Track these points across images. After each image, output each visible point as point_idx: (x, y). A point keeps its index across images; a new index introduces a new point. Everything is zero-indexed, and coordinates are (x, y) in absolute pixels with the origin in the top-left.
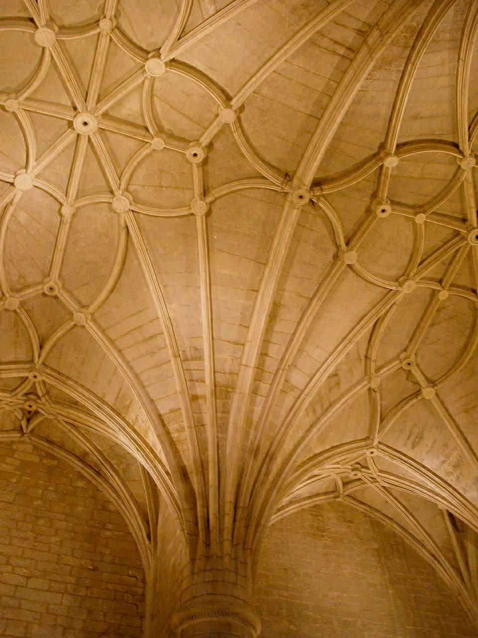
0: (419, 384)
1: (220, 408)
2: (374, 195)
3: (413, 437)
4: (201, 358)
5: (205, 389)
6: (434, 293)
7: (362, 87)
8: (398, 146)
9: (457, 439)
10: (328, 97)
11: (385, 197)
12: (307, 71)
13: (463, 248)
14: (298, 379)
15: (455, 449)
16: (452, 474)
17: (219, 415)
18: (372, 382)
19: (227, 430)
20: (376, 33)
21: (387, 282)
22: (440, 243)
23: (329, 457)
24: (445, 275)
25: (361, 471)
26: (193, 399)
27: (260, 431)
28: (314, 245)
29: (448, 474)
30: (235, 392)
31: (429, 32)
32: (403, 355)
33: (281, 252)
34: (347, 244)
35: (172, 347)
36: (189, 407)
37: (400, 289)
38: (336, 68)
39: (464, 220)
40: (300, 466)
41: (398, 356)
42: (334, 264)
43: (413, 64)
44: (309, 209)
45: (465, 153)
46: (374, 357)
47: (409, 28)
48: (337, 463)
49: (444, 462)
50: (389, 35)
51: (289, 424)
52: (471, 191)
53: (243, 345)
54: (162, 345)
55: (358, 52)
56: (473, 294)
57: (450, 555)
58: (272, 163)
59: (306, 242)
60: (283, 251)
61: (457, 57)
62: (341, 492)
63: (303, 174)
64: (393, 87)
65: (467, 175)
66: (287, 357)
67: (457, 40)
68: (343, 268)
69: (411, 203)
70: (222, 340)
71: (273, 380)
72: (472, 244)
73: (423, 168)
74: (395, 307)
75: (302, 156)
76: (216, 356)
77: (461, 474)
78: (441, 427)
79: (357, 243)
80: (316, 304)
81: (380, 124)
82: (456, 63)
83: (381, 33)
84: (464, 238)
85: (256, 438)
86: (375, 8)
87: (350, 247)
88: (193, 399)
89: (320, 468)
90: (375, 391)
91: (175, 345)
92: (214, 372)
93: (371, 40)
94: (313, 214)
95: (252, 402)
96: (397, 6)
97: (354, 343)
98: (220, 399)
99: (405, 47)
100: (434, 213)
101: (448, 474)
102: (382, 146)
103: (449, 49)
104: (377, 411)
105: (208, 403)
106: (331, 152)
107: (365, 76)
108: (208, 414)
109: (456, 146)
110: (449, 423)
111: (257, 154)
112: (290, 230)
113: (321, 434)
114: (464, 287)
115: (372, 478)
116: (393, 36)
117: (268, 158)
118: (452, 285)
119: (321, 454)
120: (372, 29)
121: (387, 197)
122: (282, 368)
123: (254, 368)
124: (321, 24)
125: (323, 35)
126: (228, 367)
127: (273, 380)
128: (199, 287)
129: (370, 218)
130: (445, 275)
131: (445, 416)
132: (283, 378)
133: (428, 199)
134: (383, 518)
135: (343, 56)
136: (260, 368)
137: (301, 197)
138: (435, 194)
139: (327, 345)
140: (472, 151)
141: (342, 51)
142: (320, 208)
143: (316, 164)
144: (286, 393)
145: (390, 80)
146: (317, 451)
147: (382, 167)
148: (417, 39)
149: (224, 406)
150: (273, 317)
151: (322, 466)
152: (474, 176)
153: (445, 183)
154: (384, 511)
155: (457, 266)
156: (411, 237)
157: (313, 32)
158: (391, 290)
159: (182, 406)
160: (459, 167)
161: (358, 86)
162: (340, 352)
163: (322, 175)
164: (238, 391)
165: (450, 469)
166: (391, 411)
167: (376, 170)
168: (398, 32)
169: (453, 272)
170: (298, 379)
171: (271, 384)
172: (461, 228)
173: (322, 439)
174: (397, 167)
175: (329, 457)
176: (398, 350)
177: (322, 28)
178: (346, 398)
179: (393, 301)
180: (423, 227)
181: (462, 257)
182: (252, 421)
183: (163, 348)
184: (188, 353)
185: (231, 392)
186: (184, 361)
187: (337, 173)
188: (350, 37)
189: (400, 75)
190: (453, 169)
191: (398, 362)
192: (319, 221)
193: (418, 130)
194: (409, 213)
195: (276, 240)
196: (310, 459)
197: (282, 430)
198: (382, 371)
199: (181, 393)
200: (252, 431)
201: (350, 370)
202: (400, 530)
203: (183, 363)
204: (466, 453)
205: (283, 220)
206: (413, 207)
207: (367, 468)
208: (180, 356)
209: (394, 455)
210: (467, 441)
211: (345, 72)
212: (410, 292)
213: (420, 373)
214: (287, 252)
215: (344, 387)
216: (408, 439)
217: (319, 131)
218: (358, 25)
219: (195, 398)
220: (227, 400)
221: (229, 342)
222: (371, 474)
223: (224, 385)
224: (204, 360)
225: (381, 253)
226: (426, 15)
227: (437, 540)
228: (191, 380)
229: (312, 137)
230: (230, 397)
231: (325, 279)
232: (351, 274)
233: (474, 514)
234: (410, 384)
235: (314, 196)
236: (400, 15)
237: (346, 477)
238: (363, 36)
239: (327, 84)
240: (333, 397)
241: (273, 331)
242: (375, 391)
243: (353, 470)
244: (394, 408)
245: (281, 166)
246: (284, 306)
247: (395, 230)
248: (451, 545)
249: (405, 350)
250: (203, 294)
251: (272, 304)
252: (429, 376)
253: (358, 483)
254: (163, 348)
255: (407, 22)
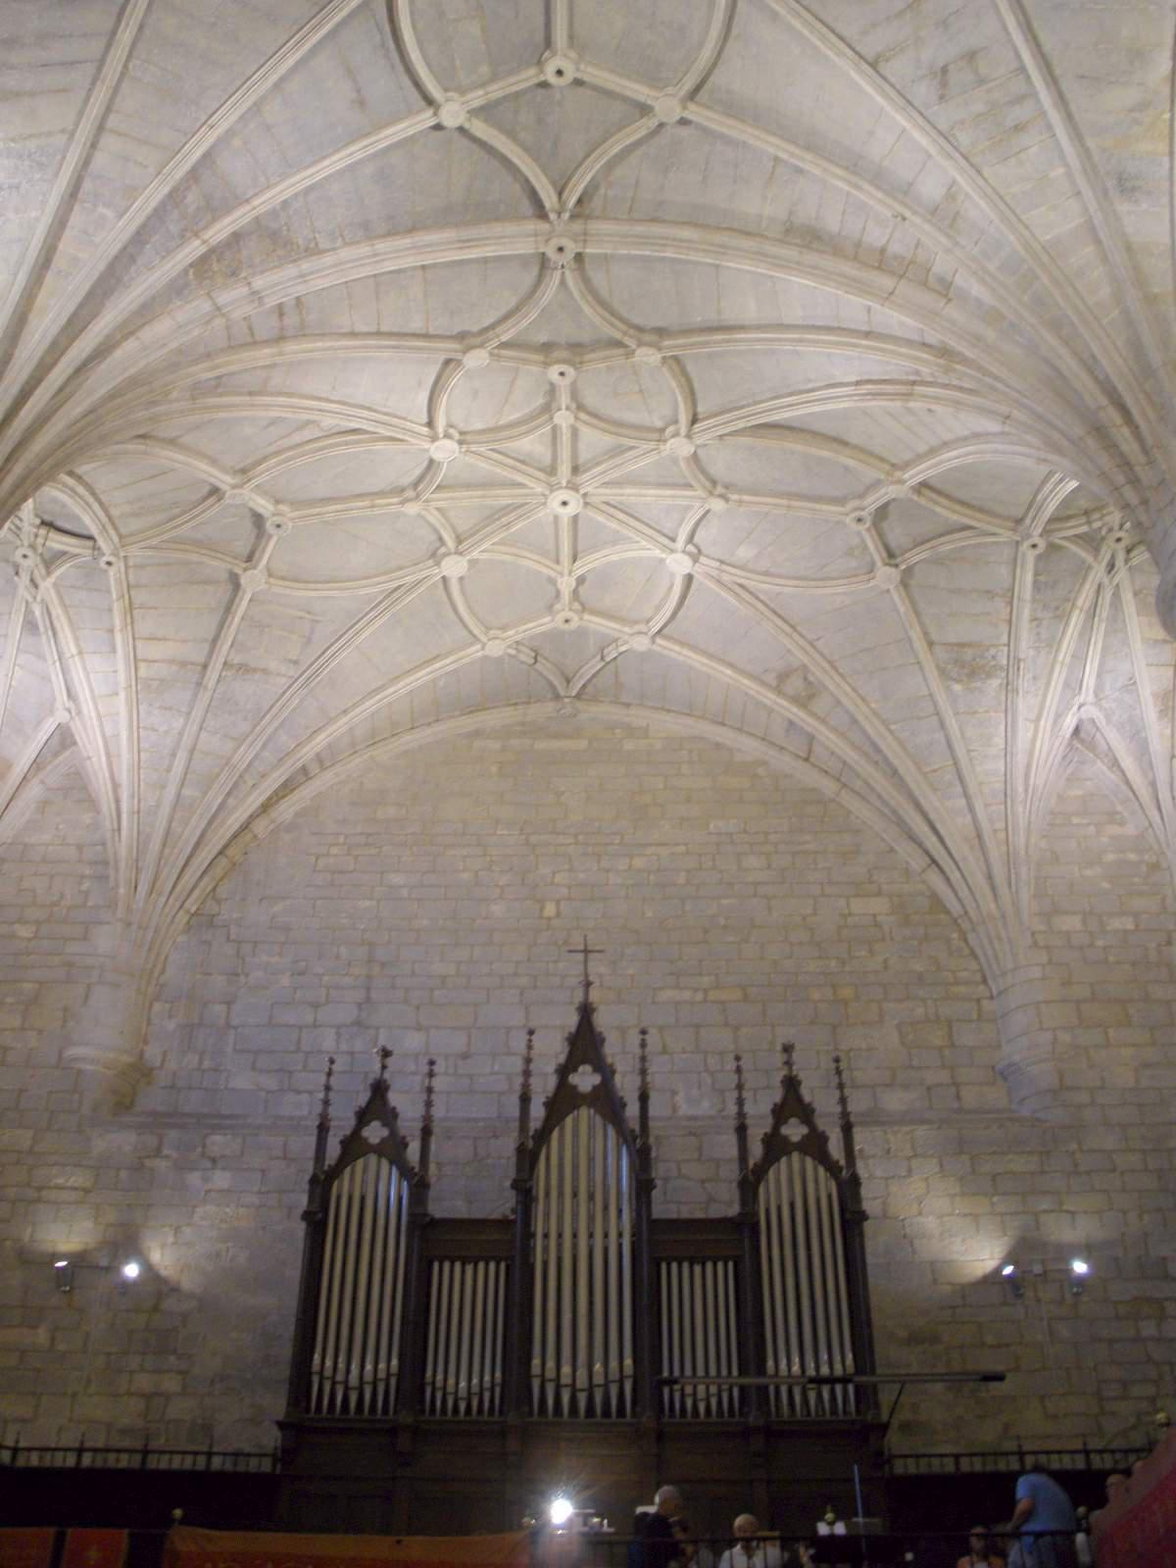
191: (479, 646)
246: (791, 213)
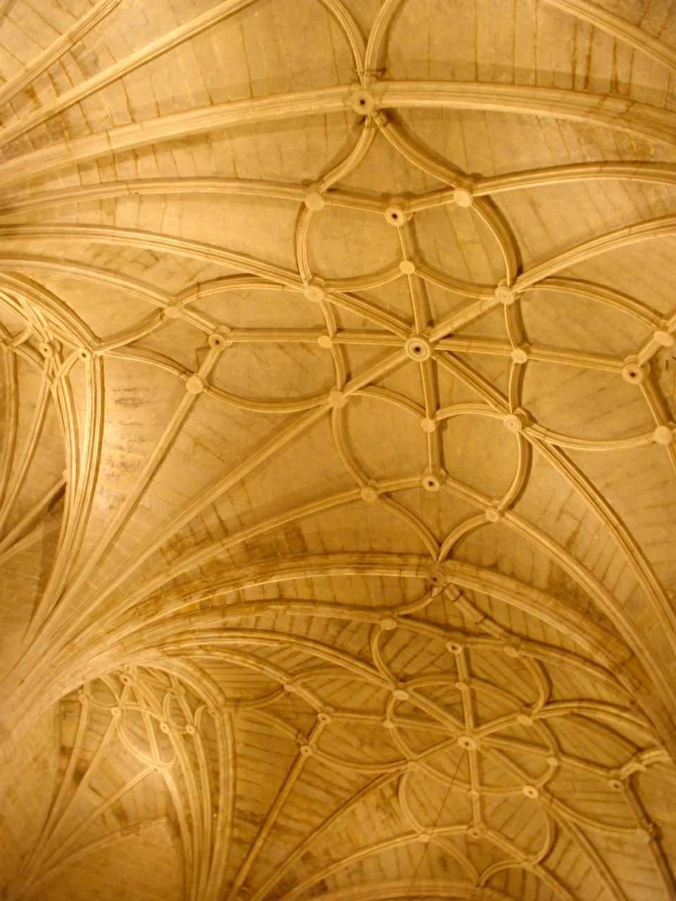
0: (199, 368)
1: (35, 134)
2: (409, 196)
3: (130, 395)
4: (87, 74)
5: (50, 101)
6: (321, 329)
7: (544, 118)
8: (487, 199)
9: (157, 450)
10: (510, 78)
11: (413, 210)
12: (535, 36)
13: (396, 337)
14: (127, 213)
15: (144, 454)
16: (113, 466)
17: (26, 137)
18: (171, 308)
19: (12, 157)
20: (621, 106)
21: (306, 263)
22: (388, 307)
23: (48, 305)
24: (351, 331)
25: (53, 355)
26: (27, 92)
27: (35, 201)
28: (308, 148)
29: (110, 460)
30: (66, 142)
31: (648, 175)
32: (224, 329)
33: (279, 111)
34: (330, 190)
35: (82, 26)
36: (15, 91)
37: (306, 283)
38: (554, 73)
39: (431, 323)
40: (18, 276)
41: (219, 323)
42: (295, 185)
43: (600, 172)
44: (352, 120)
45: (515, 286)
46: (203, 294)
47: (644, 148)
48: (48, 320)
49: (121, 448)
50: (626, 124)
51: (63, 233)
52: (471, 316)
53: (134, 121)
54: (77, 12)
55: (587, 93)
56: (345, 378)
57: (16, 516)
58: (391, 44)
59: (307, 136)
60: (280, 113)
61: (632, 223)
62: (15, 344)
63: (395, 92)
64: (562, 157)
65: (489, 301)
66: (147, 185)
67: (651, 213)
68: (297, 199)
69: (423, 244)
70: (125, 89)
71: (108, 184)
72: (406, 347)
73: (473, 242)
74: (279, 289)
75: (417, 80)
76: (100, 93)
77: (118, 476)
78: (161, 423)
79: (337, 201)
80: (233, 188)
81: (505, 164)
82: (623, 226)
83: (623, 113)
84: (408, 333)
85: (23, 200)
86: (654, 90)
87: (328, 195)
88: (27, 92)
89: (30, 301)
90: (161, 317)
91: (87, 30)
92: (78, 102)
93: (609, 103)
94: (347, 128)
95: (66, 172)
96: (669, 119)
97: (208, 261)
98: (48, 127)
99: (618, 152)
100: (422, 281)
101: (110, 460)
102: (477, 178)
103: (637, 209)
104: (139, 333)
105: (33, 114)
106: (440, 115)
107: (561, 116)
108: (20, 122)
109: (520, 271)
110: (171, 430)
111: (394, 17)
112: (313, 108)
113: (73, 280)
114: (347, 363)
115: (53, 373)
116: (628, 130)
117: (395, 36)
118: (343, 347)
119: (49, 293)
120: (626, 99)
121: (414, 213)
122: (130, 186)
123: (112, 151)
124: (606, 26)
125: (592, 36)
126: (95, 116)
127: (108, 184)
128: (179, 24)
129: (378, 204)
130: (351, 331)
131: (177, 420)
132: (119, 194)
133: (437, 266)
134: (13, 414)
135: (574, 76)
136: (115, 158)
137: (363, 102)
138: (447, 272)
139: (191, 228)
140: (522, 293)
141: (580, 71)
142: (360, 134)
143: (417, 103)
144: (101, 208)
145: (568, 151)
146: (49, 287)
147: (449, 188)
148: (634, 163)
149: (41, 137)
150: (188, 141)
151: (33, 303)
152: (492, 309)
153: (466, 278)
154: (21, 410)
155: (373, 343)
156: (377, 267)
157: (590, 21)
158: (299, 274)
159: (10, 80)
160: (495, 287)
161: (542, 113)
162: (187, 249)
163: (404, 116)
164: (70, 145)
165: (117, 460)
166: (148, 350)
167: (443, 183)
168: (634, 134)
169: (361, 339)
170: (127, 213)
171: (101, 183)
172: (420, 325)
173: (67, 284)
174: (460, 208)
175: (48, 305)
176: (227, 320)
177: (602, 31)
178: (134, 286)
179: (286, 283)
180: (399, 276)
181: (385, 342)
182: (41, 184)
183: (73, 15)
184: (84, 55)
185: (63, 136)
186: (72, 53)
187: (415, 135)
188: (603, 74)
189: (580, 161)
190: (490, 281)
192: (343, 141)
193: (518, 215)
194: (407, 251)
195: (291, 97)
196: (33, 283)
197: (52, 229)
198: (192, 314)
199: (26, 71)
200: (29, 191)
201: (171, 274)
202: (10, 440)
203: (68, 53)
204: (146, 469)
205: (321, 92)
206: (417, 251)
207: (62, 361)
208: (74, 44)
209: (95, 384)
210: (161, 461)
211: (554, 87)
212: (308, 298)
213: (213, 361)
214: (282, 117)
215: (147, 276)
216: (125, 390)
217: (462, 86)
218: (623, 79)
219: (30, 93)
220: (50, 137)
221: (128, 100)
222: (58, 369)
223: (69, 123)
224: (86, 80)
225: (339, 239)
226: (668, 161)
227: (24, 491)
228: (51, 77)
229: (448, 81)
230: (57, 139)
231: (269, 182)
232: (295, 213)
233: (80, 516)
234: (193, 357)
235: (372, 118)
236: (657, 128)
237: (36, 340)
238: (611, 92)
239: (528, 71)
240: (126, 270)
241: (171, 151)
242: (161, 317)
243: (50, 344)
244: (153, 352)
245: (392, 58)
246: (211, 146)
247: (377, 242)
248: (29, 511)
249: (232, 329)
250: (173, 34)
251: (204, 131)
252: (217, 374)
253: (37, 359)
254: (73, 15)
255: (651, 141)
